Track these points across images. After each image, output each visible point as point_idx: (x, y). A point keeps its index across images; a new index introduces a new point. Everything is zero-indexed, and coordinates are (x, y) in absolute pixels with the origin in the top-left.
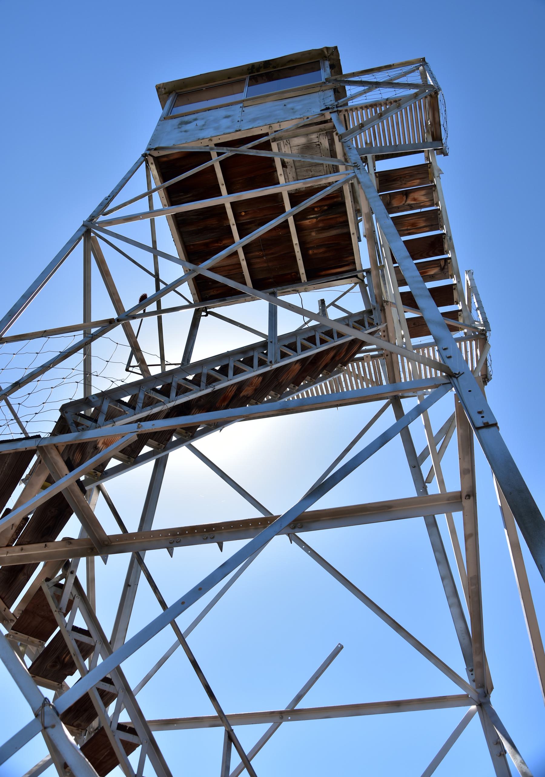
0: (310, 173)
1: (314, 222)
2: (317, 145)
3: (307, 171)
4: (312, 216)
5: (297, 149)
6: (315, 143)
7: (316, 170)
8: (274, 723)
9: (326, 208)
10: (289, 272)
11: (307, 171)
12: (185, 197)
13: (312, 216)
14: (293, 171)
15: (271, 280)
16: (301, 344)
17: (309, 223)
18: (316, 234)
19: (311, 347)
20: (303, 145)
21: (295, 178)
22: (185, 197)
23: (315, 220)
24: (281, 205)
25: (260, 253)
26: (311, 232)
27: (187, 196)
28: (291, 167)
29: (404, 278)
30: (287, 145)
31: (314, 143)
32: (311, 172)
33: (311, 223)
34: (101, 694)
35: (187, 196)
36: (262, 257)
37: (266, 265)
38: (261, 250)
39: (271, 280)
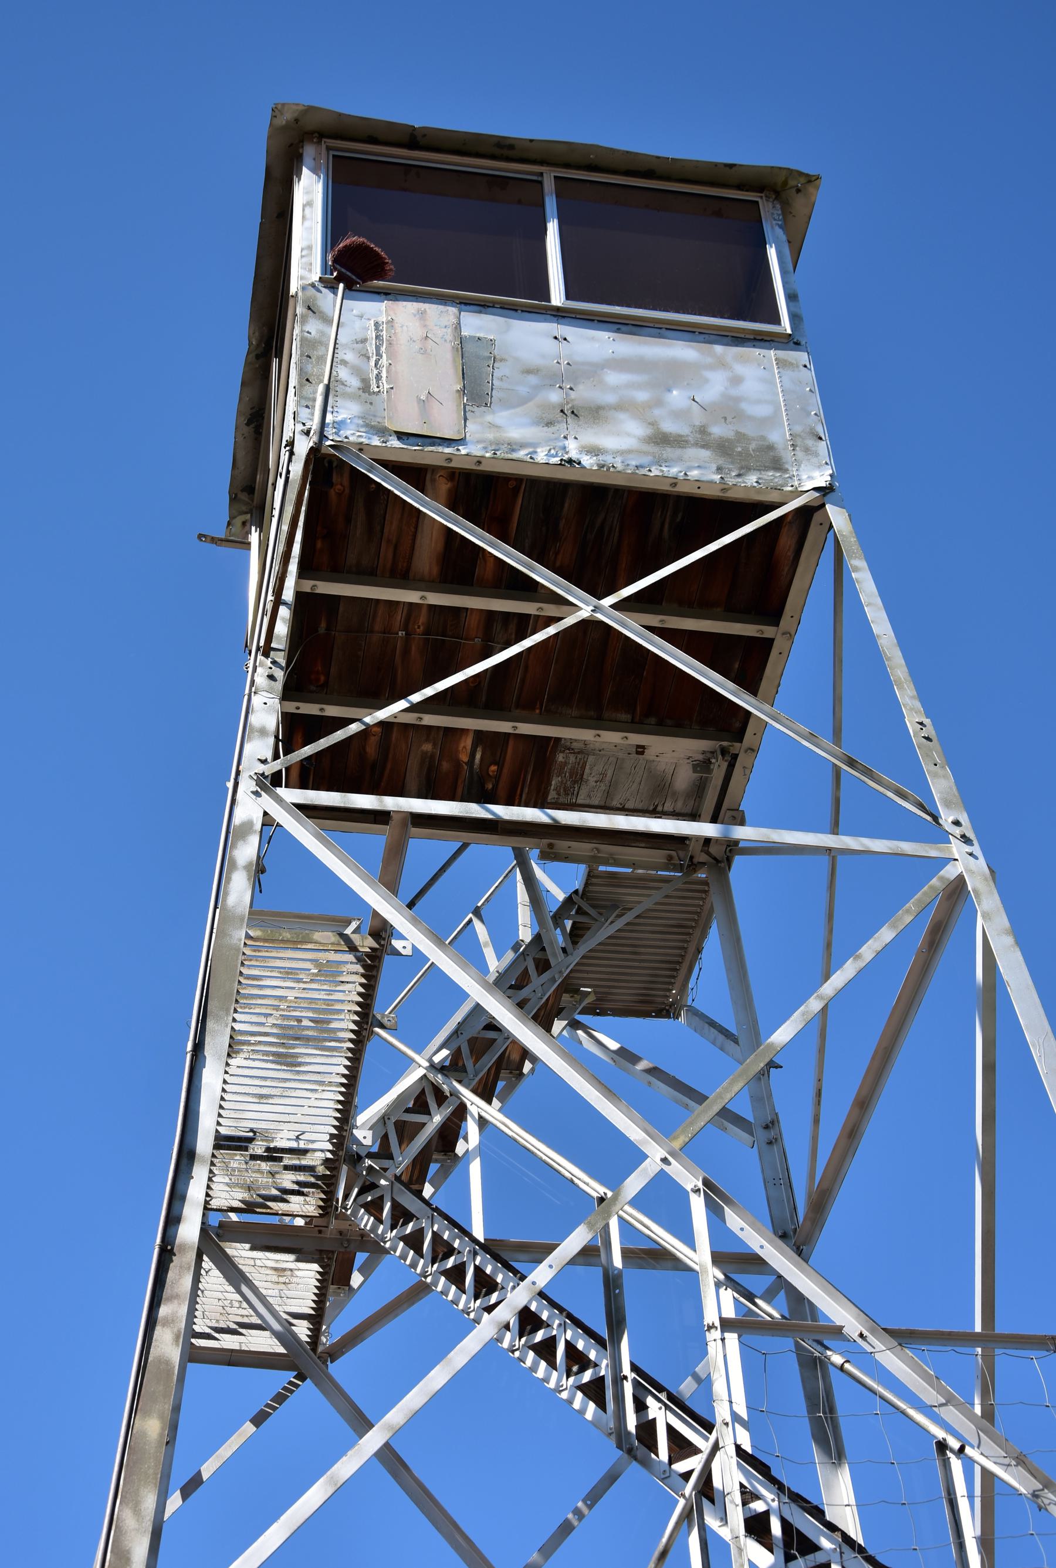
0: (595, 779)
1: (460, 756)
2: (657, 806)
3: (604, 775)
4: (478, 756)
5: (666, 770)
6: (664, 804)
7: (596, 790)
8: (738, 810)
9: (486, 786)
10: (334, 670)
11: (604, 775)
12: (668, 521)
13: (478, 756)
14: (619, 754)
15: (323, 625)
16: (274, 761)
17: (462, 745)
18: (424, 754)
19: (188, 1264)
20: (667, 784)
21: (598, 752)
22: (668, 521)
23: (464, 758)
24: (538, 706)
25: (419, 627)
26: (435, 745)
27: (666, 526)
28: (631, 752)
29: (573, 1401)
30: (688, 759)
31: (663, 802)
32: (596, 782)
33: (460, 749)
34: (585, 961)
35: (666, 526)
36: (406, 628)
37: (378, 626)
38: (427, 632)
39: (323, 625)
